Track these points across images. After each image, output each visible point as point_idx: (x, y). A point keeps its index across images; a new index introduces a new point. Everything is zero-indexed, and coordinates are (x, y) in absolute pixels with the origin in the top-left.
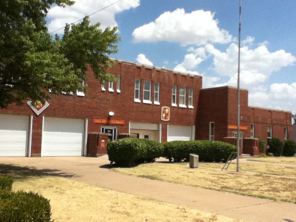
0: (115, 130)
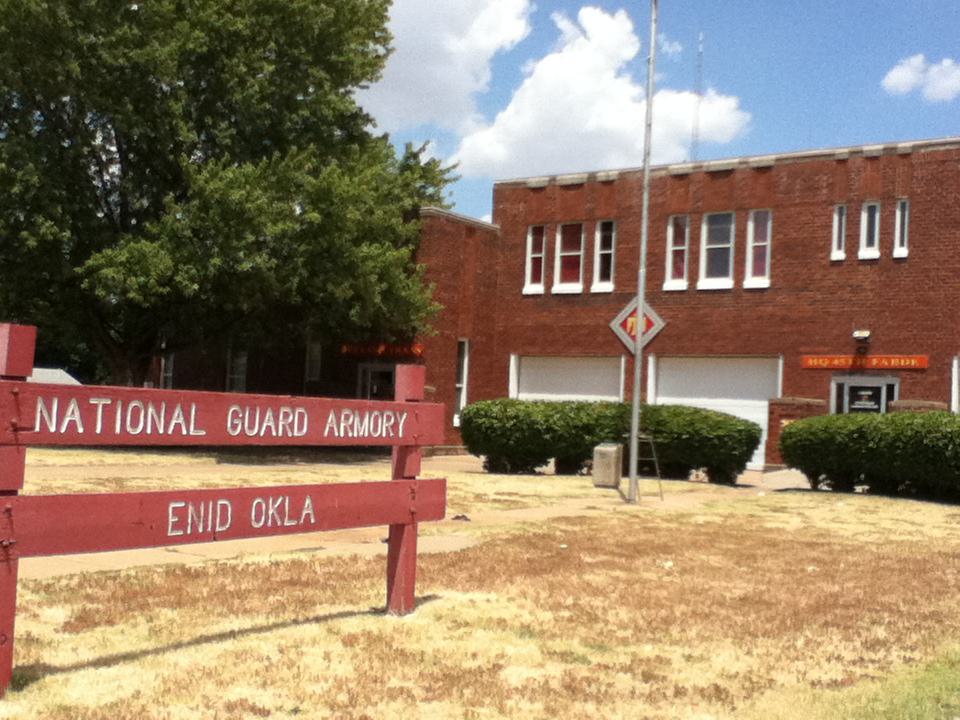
0: (890, 388)
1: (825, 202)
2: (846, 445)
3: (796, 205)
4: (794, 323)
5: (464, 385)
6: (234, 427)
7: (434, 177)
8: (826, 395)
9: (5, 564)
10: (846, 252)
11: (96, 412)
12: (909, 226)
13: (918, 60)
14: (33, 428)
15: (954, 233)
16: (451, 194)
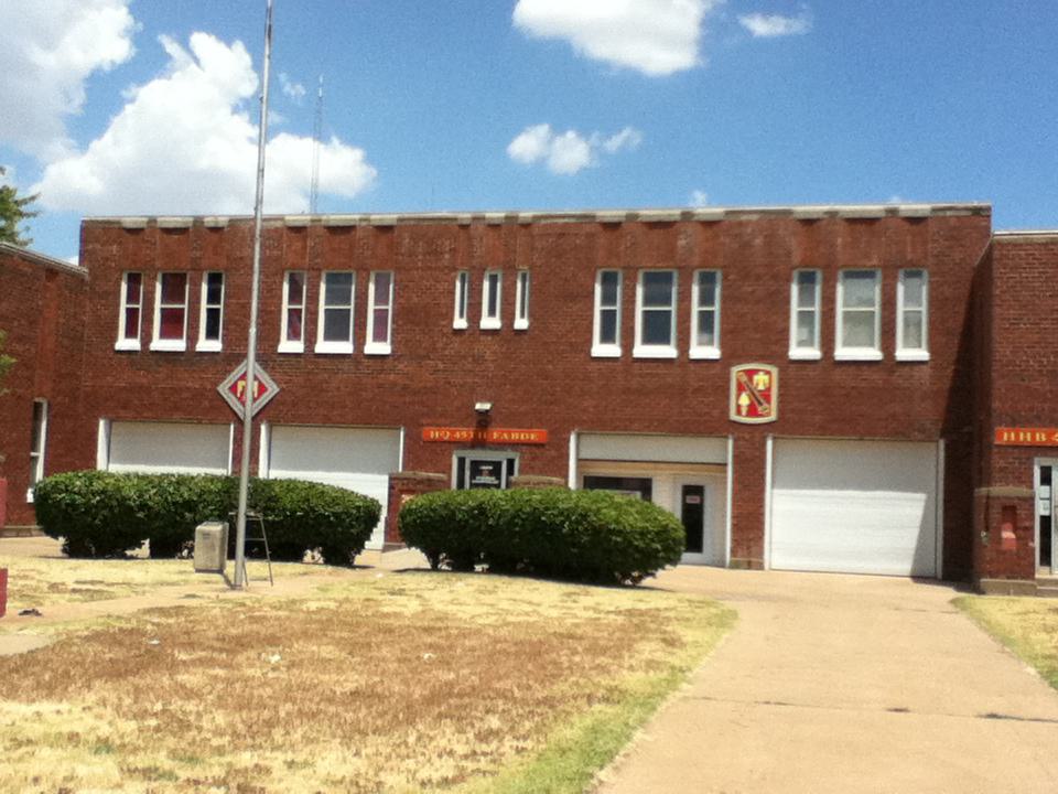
0: (511, 463)
2: (467, 521)
5: (41, 454)
13: (543, 130)
16: (28, 229)
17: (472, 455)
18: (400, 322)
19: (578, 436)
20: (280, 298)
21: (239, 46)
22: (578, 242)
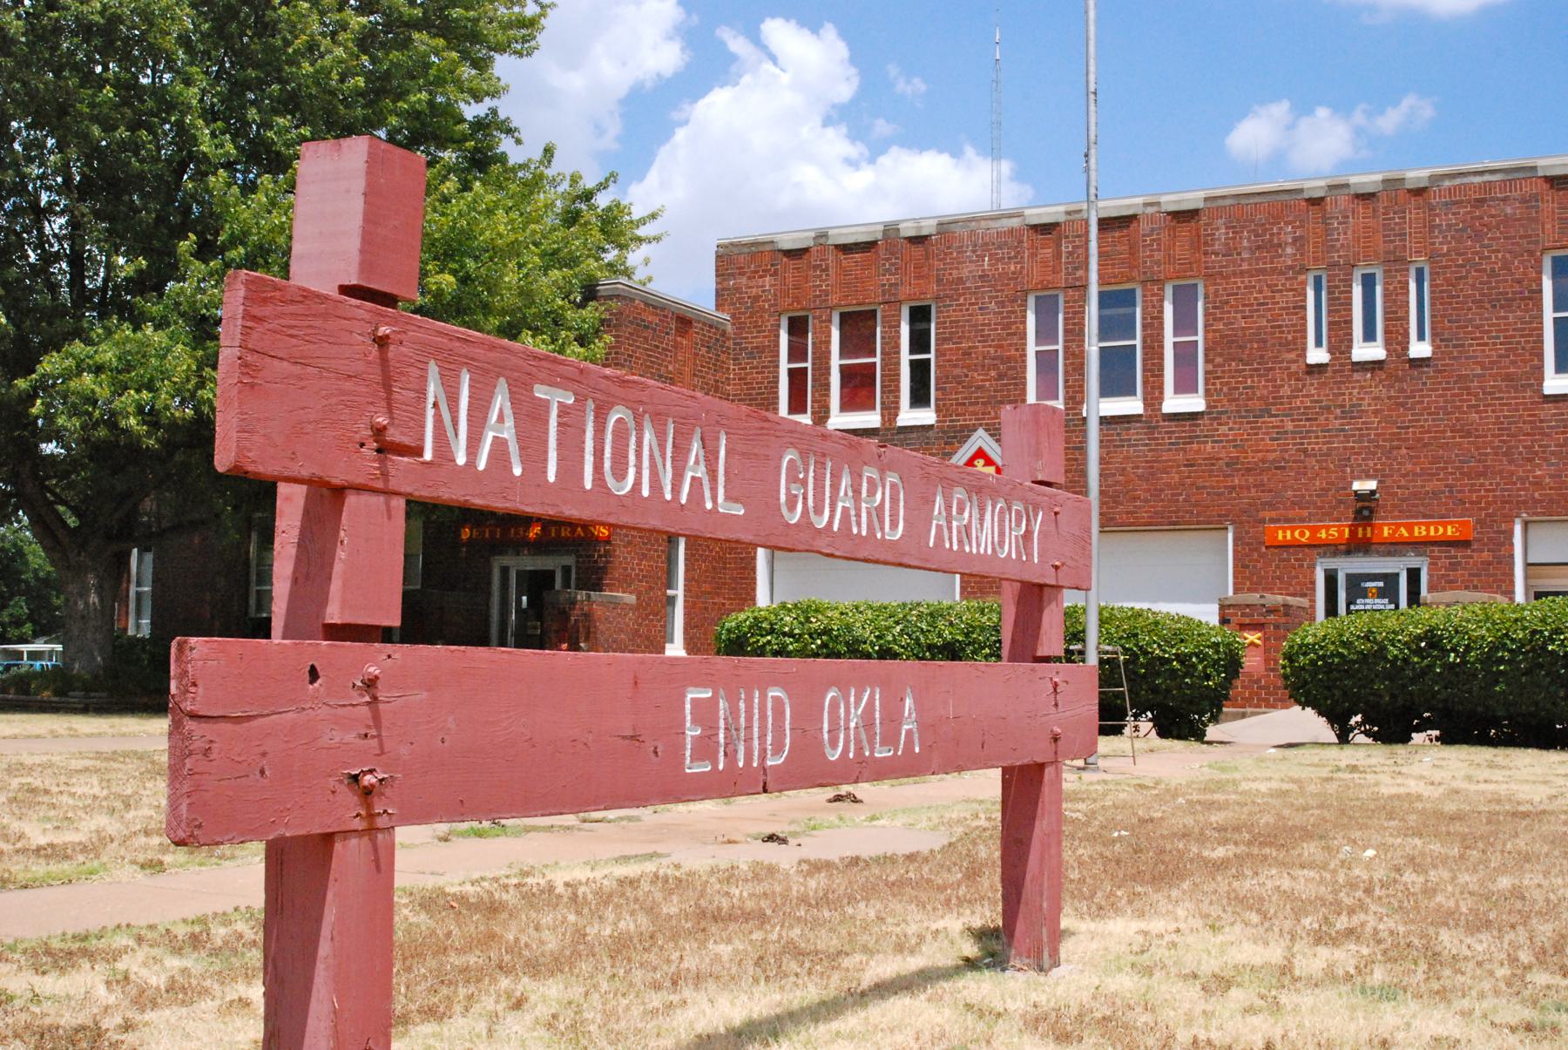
0: (1414, 575)
1: (1291, 267)
2: (1405, 660)
3: (1242, 273)
4: (1249, 470)
5: (679, 592)
6: (792, 506)
7: (622, 233)
8: (1308, 590)
9: (366, 839)
10: (1330, 351)
11: (547, 411)
12: (1432, 305)
13: (1280, 110)
14: (419, 451)
15: (1506, 318)
16: (647, 262)
17: (1347, 566)
18: (1219, 360)
19: (1526, 524)
20: (1024, 336)
21: (830, 32)
22: (1509, 210)
